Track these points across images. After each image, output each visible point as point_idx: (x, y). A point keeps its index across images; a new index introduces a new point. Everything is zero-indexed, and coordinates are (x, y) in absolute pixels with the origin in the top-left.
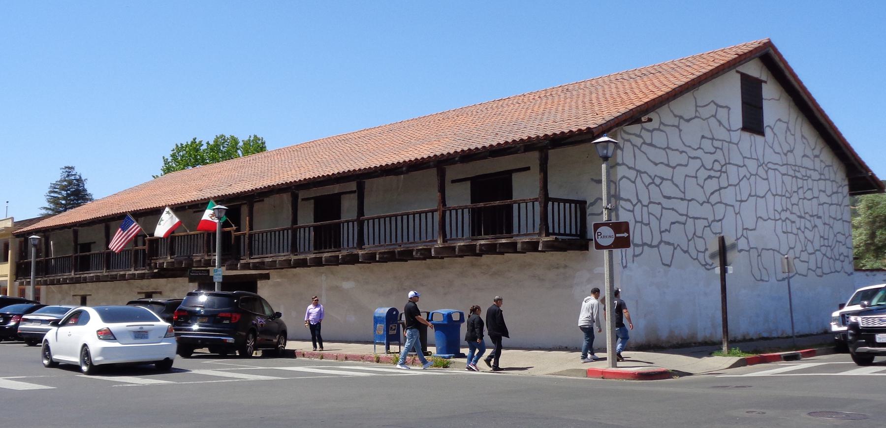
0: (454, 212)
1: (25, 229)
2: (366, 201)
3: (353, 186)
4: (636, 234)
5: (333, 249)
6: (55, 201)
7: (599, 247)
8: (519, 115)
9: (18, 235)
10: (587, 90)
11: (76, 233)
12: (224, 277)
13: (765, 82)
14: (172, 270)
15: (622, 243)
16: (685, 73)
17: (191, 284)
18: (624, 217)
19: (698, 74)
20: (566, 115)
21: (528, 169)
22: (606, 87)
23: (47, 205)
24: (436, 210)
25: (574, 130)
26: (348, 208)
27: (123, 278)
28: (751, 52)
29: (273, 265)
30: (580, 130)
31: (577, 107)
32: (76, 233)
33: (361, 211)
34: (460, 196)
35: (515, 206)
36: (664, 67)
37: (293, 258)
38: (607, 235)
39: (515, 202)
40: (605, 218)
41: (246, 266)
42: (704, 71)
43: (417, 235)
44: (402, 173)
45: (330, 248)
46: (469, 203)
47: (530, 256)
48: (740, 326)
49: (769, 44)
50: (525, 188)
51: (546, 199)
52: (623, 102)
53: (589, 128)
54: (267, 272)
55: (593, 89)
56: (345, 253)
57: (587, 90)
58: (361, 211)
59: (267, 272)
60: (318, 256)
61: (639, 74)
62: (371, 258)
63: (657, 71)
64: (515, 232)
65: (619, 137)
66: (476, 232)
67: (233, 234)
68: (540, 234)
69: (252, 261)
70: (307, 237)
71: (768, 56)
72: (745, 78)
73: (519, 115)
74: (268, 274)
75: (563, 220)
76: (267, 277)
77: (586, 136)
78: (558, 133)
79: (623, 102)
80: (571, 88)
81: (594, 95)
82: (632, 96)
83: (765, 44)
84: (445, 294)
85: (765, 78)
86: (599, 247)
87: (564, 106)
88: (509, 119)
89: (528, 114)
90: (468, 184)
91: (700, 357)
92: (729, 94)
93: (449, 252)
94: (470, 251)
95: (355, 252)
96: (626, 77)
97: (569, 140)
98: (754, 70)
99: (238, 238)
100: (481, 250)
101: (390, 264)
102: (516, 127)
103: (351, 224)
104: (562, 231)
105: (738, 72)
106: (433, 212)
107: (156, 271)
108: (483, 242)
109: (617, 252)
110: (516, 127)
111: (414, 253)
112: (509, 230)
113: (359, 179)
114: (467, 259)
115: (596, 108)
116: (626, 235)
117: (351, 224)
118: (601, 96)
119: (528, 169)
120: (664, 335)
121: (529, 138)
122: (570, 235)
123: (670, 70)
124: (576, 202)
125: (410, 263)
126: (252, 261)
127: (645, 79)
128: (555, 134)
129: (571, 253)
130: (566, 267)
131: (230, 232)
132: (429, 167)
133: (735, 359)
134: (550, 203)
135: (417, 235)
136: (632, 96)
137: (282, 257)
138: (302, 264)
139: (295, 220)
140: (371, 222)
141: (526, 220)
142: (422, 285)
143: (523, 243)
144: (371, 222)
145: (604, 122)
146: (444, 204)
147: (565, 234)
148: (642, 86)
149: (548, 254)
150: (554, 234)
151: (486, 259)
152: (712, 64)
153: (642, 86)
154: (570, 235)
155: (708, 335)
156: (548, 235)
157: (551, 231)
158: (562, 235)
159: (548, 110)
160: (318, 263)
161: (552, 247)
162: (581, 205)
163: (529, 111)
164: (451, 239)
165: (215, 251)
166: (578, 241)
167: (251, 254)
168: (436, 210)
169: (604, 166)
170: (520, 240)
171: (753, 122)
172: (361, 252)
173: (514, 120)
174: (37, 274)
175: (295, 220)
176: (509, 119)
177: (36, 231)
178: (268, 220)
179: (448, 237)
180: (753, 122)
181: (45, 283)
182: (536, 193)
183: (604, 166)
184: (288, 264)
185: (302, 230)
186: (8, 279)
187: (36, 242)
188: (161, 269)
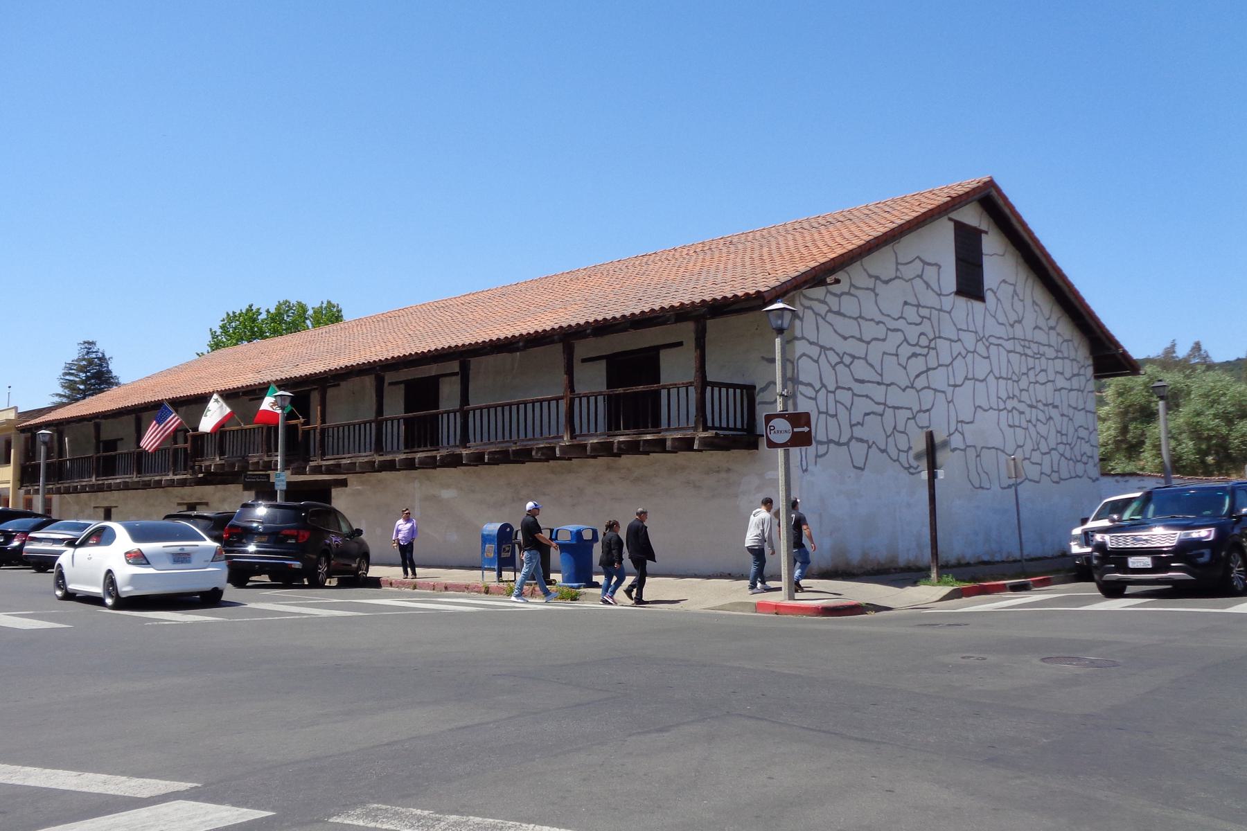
0: (584, 400)
1: (33, 422)
3: (455, 366)
4: (819, 429)
6: (70, 385)
7: (772, 445)
9: (23, 430)
11: (98, 427)
12: (289, 484)
13: (986, 233)
14: (222, 474)
16: (883, 221)
17: (246, 493)
18: (803, 406)
20: (729, 275)
21: (680, 344)
23: (61, 391)
24: (562, 398)
25: (740, 294)
26: (449, 395)
27: (158, 484)
29: (351, 469)
30: (747, 294)
31: (744, 265)
34: (593, 379)
35: (664, 393)
37: (378, 459)
41: (317, 470)
47: (682, 457)
48: (954, 547)
49: (991, 184)
50: (676, 369)
52: (802, 258)
53: (758, 292)
54: (344, 477)
55: (764, 242)
56: (444, 452)
57: (757, 244)
59: (344, 477)
60: (410, 456)
61: (824, 222)
62: (478, 460)
63: (847, 218)
64: (664, 425)
68: (695, 429)
70: (395, 432)
71: (989, 199)
72: (960, 228)
75: (725, 410)
76: (344, 483)
79: (802, 258)
80: (735, 240)
82: (815, 251)
86: (772, 445)
90: (603, 364)
92: (940, 246)
93: (578, 451)
94: (605, 450)
95: (458, 451)
96: (806, 225)
98: (972, 216)
100: (619, 448)
101: (502, 466)
102: (665, 290)
104: (724, 425)
105: (950, 219)
106: (557, 399)
108: (622, 439)
109: (795, 451)
110: (665, 290)
112: (656, 423)
113: (464, 356)
116: (806, 429)
117: (452, 415)
119: (680, 344)
120: (855, 558)
121: (682, 304)
122: (735, 429)
124: (742, 387)
127: (831, 228)
130: (728, 470)
132: (552, 342)
133: (946, 590)
134: (709, 389)
136: (815, 251)
137: (363, 458)
138: (389, 466)
139: (380, 411)
141: (678, 410)
142: (544, 494)
146: (572, 391)
147: (728, 429)
148: (827, 237)
149: (706, 454)
150: (713, 428)
151: (626, 460)
152: (917, 209)
153: (827, 237)
154: (735, 429)
155: (912, 558)
156: (706, 429)
157: (709, 424)
160: (410, 465)
161: (709, 445)
162: (749, 392)
163: (682, 270)
164: (581, 435)
166: (744, 437)
167: (323, 454)
168: (562, 398)
170: (670, 436)
171: (970, 284)
172: (465, 452)
175: (380, 411)
179: (578, 432)
180: (970, 284)
182: (691, 375)
184: (371, 468)
186: (10, 485)
187: (47, 439)
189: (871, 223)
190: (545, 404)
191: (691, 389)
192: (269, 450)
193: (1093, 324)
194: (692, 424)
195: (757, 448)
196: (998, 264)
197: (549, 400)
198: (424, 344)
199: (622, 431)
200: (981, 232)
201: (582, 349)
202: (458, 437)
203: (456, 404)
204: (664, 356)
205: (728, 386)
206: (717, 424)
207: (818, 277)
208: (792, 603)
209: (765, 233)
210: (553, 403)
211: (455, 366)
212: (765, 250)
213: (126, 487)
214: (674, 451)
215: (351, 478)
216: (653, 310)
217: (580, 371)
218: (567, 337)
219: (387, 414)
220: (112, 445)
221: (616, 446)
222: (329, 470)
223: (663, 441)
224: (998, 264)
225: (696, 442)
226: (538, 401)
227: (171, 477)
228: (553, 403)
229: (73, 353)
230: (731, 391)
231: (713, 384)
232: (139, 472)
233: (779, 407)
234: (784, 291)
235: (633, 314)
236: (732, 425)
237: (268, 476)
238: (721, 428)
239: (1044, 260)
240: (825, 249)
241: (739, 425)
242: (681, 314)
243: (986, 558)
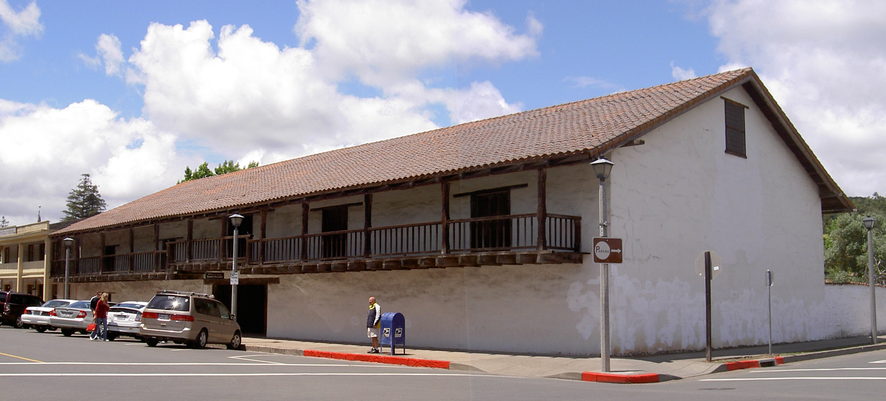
0: (457, 225)
1: (59, 232)
2: (373, 212)
3: (361, 198)
4: (626, 251)
5: (497, 248)
6: (73, 206)
7: (597, 260)
8: (516, 133)
9: (52, 237)
10: (581, 112)
11: (103, 236)
12: (240, 280)
13: (748, 108)
14: (190, 272)
15: (616, 258)
16: (674, 99)
17: (206, 286)
18: (614, 235)
19: (686, 100)
20: (562, 136)
21: (526, 185)
22: (599, 108)
23: (67, 209)
24: (440, 223)
25: (572, 151)
26: (356, 221)
27: (146, 278)
28: (734, 79)
29: (286, 271)
30: (577, 151)
31: (573, 129)
32: (157, 229)
33: (368, 223)
34: (462, 210)
35: (514, 221)
36: (653, 91)
37: (304, 264)
38: (604, 250)
39: (514, 216)
40: (601, 234)
41: (259, 271)
42: (692, 97)
43: (422, 246)
44: (408, 187)
45: (339, 255)
46: (469, 216)
47: (527, 268)
48: (723, 335)
49: (751, 73)
50: (522, 204)
51: (543, 215)
52: (616, 125)
53: (586, 150)
54: (277, 276)
55: (586, 110)
56: (352, 260)
57: (581, 112)
58: (368, 223)
59: (277, 276)
60: (327, 263)
61: (630, 97)
62: (378, 267)
63: (645, 95)
64: (514, 244)
65: (613, 158)
66: (475, 244)
67: (248, 241)
68: (537, 247)
69: (264, 266)
70: (315, 246)
71: (750, 85)
72: (729, 104)
73: (516, 133)
74: (278, 279)
75: (559, 235)
76: (276, 281)
77: (586, 156)
78: (556, 153)
79: (616, 125)
80: (565, 108)
81: (588, 117)
82: (625, 119)
83: (747, 72)
84: (446, 301)
85: (747, 105)
86: (597, 260)
87: (559, 127)
88: (507, 138)
89: (525, 133)
90: (469, 198)
91: (659, 362)
92: (714, 119)
93: (453, 262)
94: (472, 262)
95: (362, 259)
96: (616, 98)
97: (565, 160)
98: (738, 97)
99: (251, 245)
100: (463, 261)
101: (394, 272)
102: (515, 146)
103: (358, 234)
104: (558, 245)
105: (722, 98)
106: (437, 224)
107: (175, 273)
108: (483, 254)
109: (613, 267)
110: (515, 146)
111: (419, 262)
112: (508, 243)
113: (368, 191)
114: (466, 269)
115: (591, 130)
116: (619, 251)
117: (358, 234)
118: (594, 117)
119: (526, 185)
120: (650, 343)
121: (529, 157)
122: (566, 248)
123: (659, 94)
124: (572, 218)
125: (413, 272)
126: (264, 266)
127: (636, 101)
128: (553, 154)
129: (565, 265)
130: (560, 278)
131: (244, 239)
132: (434, 182)
133: (717, 365)
134: (548, 219)
135: (422, 246)
136: (625, 119)
137: (293, 263)
138: (312, 270)
139: (305, 229)
140: (378, 232)
141: (524, 233)
142: (424, 292)
143: (522, 255)
144: (378, 232)
145: (600, 144)
146: (448, 218)
147: (561, 248)
148: (633, 109)
149: (544, 266)
150: (551, 247)
151: (484, 269)
152: (698, 90)
153: (633, 109)
154: (566, 248)
155: (691, 343)
156: (545, 248)
157: (548, 244)
158: (558, 248)
159: (544, 130)
160: (328, 269)
161: (547, 260)
162: (576, 222)
163: (526, 130)
164: (454, 250)
165: (231, 255)
166: (573, 254)
167: (263, 260)
168: (440, 223)
169: (601, 187)
170: (519, 253)
171: (736, 145)
172: (368, 261)
173: (512, 139)
174: (70, 274)
175: (305, 229)
176: (507, 138)
177: (69, 234)
178: (277, 229)
179: (451, 248)
180: (736, 145)
181: (77, 281)
182: (535, 208)
183: (601, 187)
184: (299, 270)
185: (312, 239)
186: (44, 276)
187: (69, 243)
188: (181, 271)
189: (665, 99)
190: (428, 227)
191: (535, 219)
192: (224, 256)
194: (535, 244)
195: (582, 263)
196: (754, 127)
197: (431, 225)
199: (504, 247)
200: (744, 107)
201: (455, 188)
202: (363, 250)
203: (362, 226)
204: (513, 193)
206: (553, 245)
207: (629, 139)
208: (608, 373)
209: (586, 103)
210: (434, 227)
211: (361, 198)
212: (588, 117)
213: (124, 279)
214: (388, 268)
215: (282, 277)
216: (507, 161)
217: (453, 204)
218: (446, 179)
219: (311, 232)
220: (110, 250)
221: (479, 259)
222: (268, 272)
223: (456, 259)
224: (754, 127)
225: (538, 258)
226: (422, 225)
227: (154, 273)
228: (434, 227)
229: (75, 185)
232: (132, 269)
233: (601, 234)
234: (603, 150)
235: (492, 164)
236: (564, 246)
237: (223, 274)
238: (556, 248)
239: (787, 128)
240: (633, 119)
241: (569, 246)
242: (528, 164)
243: (743, 344)
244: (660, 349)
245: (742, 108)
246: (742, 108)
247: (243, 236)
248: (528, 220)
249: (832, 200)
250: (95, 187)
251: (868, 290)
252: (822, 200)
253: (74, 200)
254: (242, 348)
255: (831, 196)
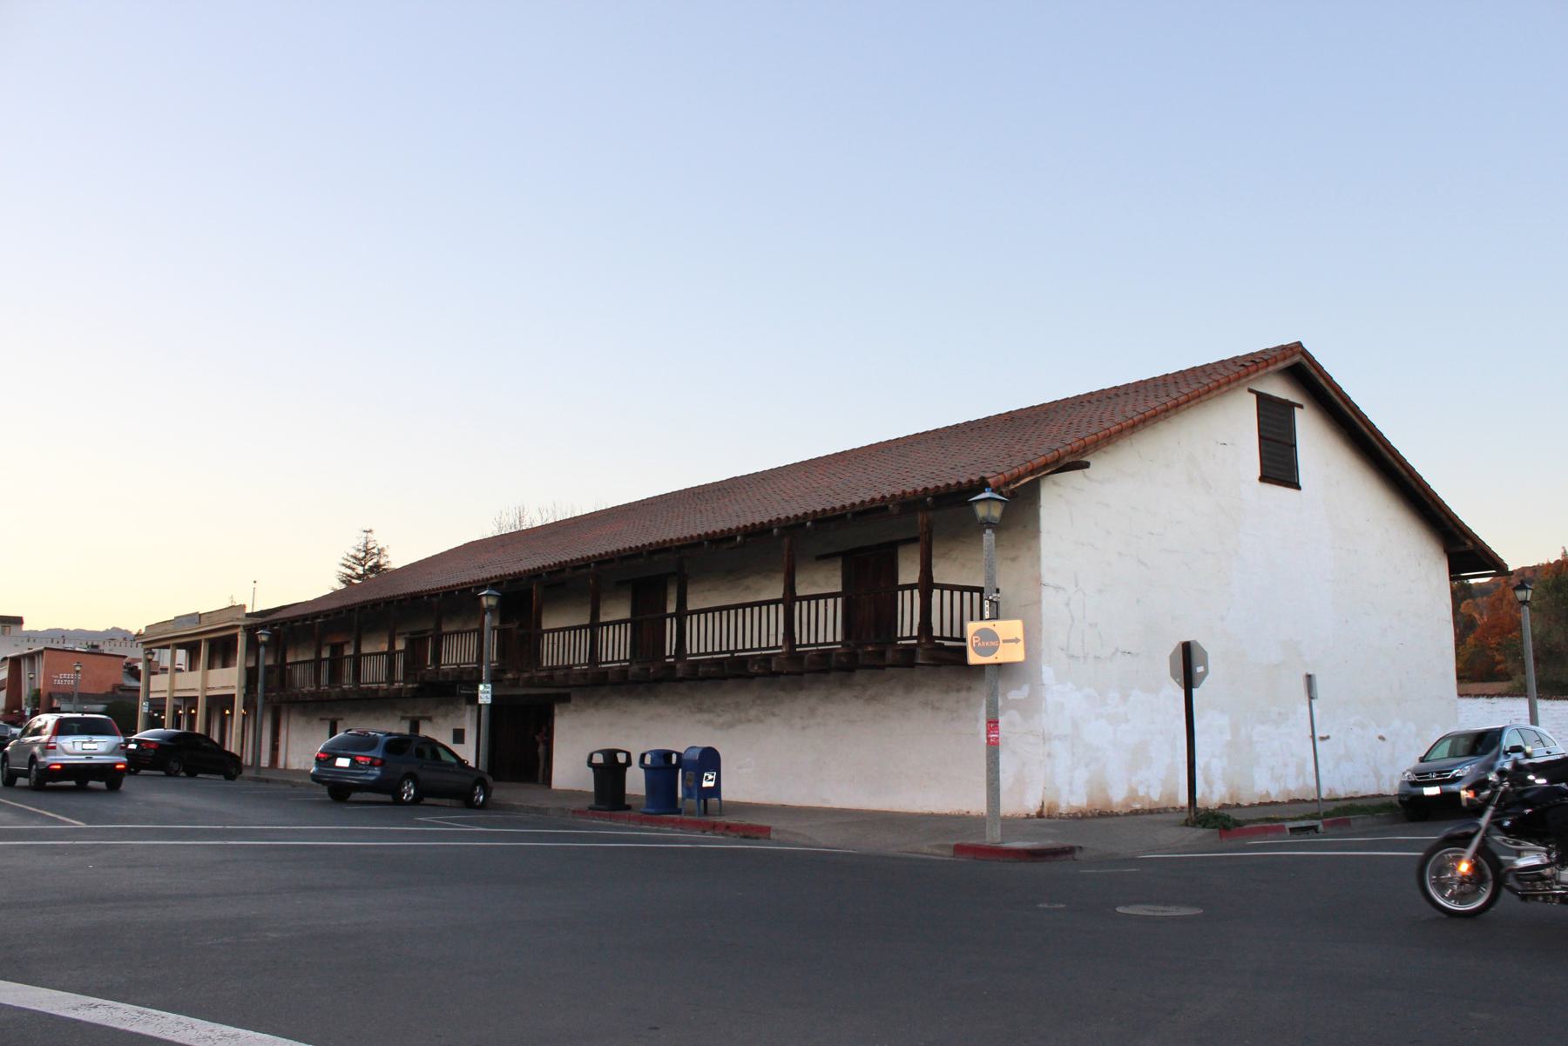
13: (1301, 407)
71: (1302, 370)
72: (1264, 401)
92: (1234, 426)
104: (756, 645)
105: (1251, 391)
134: (936, 593)
171: (1279, 466)
180: (1279, 466)
193: (1443, 516)
196: (1312, 439)
198: (795, 506)
199: (141, 685)
200: (1292, 405)
202: (781, 637)
205: (962, 589)
224: (1312, 439)
229: (351, 544)
230: (967, 595)
231: (943, 587)
244: (1138, 806)
245: (1289, 407)
246: (1289, 407)
247: (508, 626)
248: (773, 607)
249: (1463, 551)
250: (380, 551)
251: (1008, 807)
252: (1446, 551)
253: (349, 572)
254: (499, 807)
255: (1462, 549)
